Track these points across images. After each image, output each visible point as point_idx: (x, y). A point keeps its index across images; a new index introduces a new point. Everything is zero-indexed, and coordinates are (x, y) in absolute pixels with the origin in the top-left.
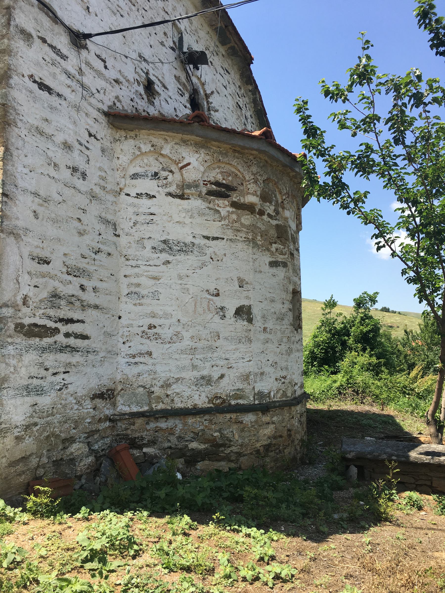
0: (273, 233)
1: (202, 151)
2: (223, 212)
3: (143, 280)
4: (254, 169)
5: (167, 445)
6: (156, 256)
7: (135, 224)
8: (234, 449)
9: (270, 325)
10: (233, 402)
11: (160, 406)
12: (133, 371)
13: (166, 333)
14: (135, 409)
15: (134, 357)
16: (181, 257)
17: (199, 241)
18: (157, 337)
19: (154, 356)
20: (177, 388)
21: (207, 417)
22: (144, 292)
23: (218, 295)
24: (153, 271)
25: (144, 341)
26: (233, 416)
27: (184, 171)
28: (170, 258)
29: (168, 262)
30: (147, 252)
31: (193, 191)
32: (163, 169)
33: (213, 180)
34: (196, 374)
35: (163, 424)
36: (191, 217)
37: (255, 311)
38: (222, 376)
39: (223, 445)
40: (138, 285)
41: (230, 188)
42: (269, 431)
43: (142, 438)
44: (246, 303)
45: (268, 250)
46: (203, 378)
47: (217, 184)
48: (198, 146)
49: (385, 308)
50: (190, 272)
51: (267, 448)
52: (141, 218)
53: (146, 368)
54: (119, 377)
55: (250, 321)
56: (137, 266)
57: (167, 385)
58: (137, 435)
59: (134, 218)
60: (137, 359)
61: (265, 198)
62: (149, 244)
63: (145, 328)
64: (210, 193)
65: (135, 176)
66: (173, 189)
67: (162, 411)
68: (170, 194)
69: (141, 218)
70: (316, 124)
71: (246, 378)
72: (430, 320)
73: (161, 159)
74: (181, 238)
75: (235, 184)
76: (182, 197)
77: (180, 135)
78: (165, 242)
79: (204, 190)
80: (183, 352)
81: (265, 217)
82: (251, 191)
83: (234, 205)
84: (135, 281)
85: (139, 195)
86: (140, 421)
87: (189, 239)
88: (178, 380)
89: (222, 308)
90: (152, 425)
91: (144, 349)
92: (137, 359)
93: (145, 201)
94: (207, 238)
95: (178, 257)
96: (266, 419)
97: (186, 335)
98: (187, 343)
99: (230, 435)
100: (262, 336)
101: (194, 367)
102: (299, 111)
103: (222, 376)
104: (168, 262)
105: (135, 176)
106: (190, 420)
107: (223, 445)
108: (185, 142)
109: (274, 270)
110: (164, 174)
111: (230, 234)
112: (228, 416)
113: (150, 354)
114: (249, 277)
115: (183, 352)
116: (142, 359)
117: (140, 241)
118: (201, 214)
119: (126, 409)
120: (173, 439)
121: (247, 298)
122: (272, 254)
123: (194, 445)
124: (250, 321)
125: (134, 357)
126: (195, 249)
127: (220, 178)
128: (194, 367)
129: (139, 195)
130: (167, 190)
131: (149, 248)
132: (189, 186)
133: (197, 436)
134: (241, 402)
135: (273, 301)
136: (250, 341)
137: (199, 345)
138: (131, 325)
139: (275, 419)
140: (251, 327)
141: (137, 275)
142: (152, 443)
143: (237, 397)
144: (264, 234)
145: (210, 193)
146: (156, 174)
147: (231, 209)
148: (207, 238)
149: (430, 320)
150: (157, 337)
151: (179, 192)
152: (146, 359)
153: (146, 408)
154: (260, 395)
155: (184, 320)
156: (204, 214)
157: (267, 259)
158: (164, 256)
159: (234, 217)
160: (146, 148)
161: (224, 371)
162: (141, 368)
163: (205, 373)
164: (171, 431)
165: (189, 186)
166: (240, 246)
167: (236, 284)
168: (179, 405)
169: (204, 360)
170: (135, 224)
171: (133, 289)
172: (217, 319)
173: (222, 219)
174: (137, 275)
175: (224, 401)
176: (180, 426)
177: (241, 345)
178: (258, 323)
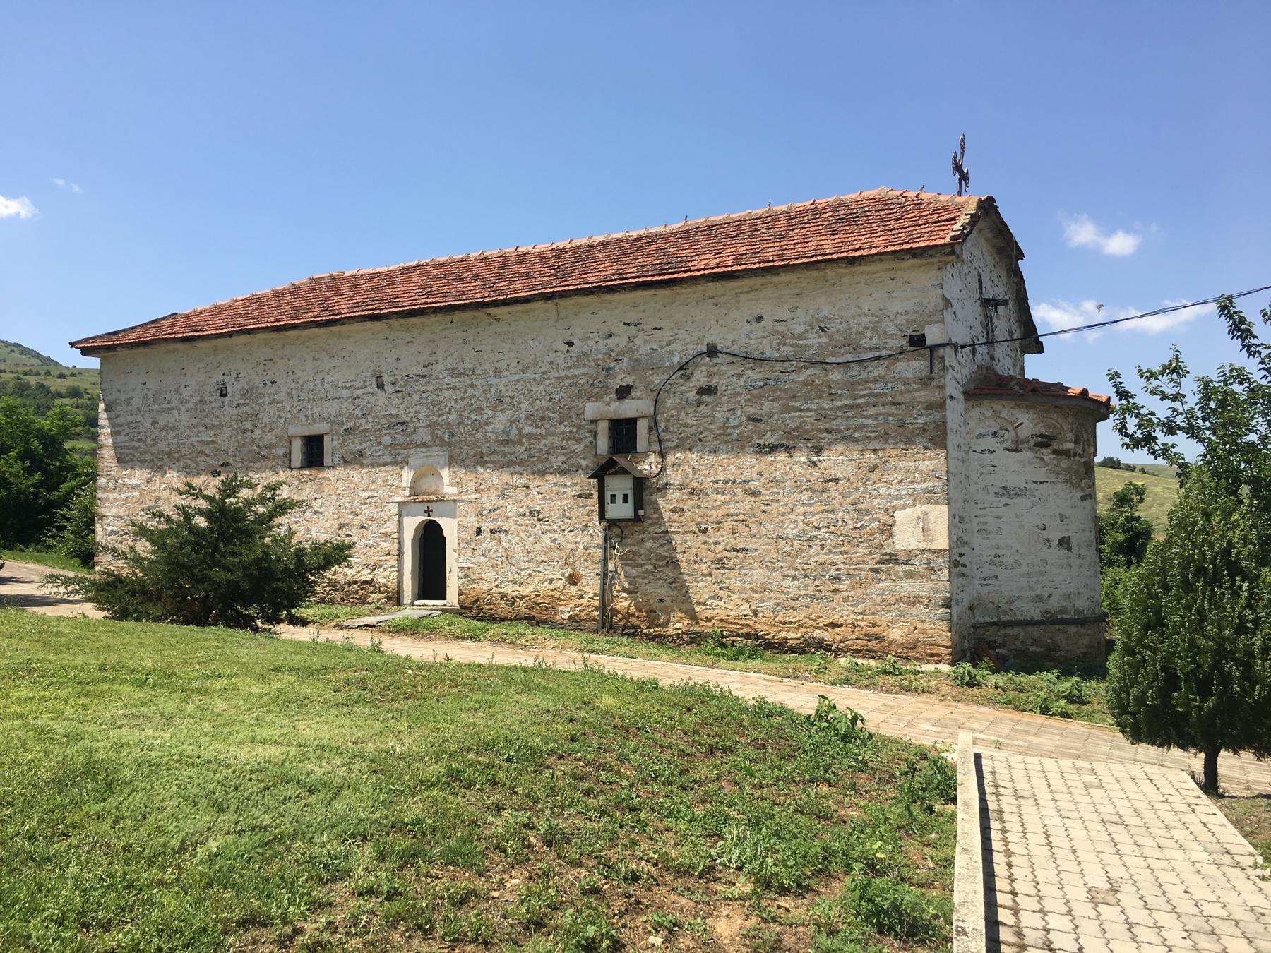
0: (1082, 470)
1: (1031, 412)
2: (1047, 460)
3: (988, 519)
4: (1070, 420)
5: (1013, 647)
6: (998, 499)
7: (981, 475)
8: (1063, 653)
9: (1082, 552)
10: (1059, 617)
11: (1006, 618)
12: (984, 590)
13: (1008, 561)
14: (988, 620)
15: (985, 579)
16: (1017, 500)
17: (1029, 486)
18: (1001, 564)
19: (1000, 578)
20: (1017, 604)
21: (1042, 627)
22: (990, 529)
23: (1045, 529)
24: (997, 512)
25: (991, 567)
26: (1061, 627)
27: (1018, 429)
28: (1009, 501)
29: (1007, 504)
30: (992, 497)
31: (1026, 445)
32: (1001, 429)
33: (1038, 433)
34: (1034, 594)
35: (1010, 632)
36: (1024, 467)
37: (1074, 542)
38: (1050, 595)
39: (1053, 650)
40: (985, 523)
41: (1052, 438)
42: (1085, 641)
43: (996, 642)
44: (1066, 534)
45: (1080, 486)
46: (1037, 596)
47: (1042, 436)
48: (1029, 408)
49: (1111, 459)
50: (1024, 512)
51: (1085, 654)
52: (985, 470)
53: (994, 588)
54: (975, 595)
55: (1070, 549)
56: (984, 508)
57: (1010, 602)
58: (991, 639)
59: (981, 470)
60: (987, 582)
61: (1076, 442)
62: (992, 491)
63: (992, 557)
64: (1036, 445)
65: (980, 436)
66: (1009, 444)
67: (1008, 621)
68: (1007, 449)
69: (985, 470)
70: (1128, 389)
71: (1068, 596)
72: (237, 707)
73: (999, 420)
74: (1017, 485)
75: (1055, 434)
76: (1016, 450)
77: (1013, 402)
78: (1004, 488)
79: (1032, 443)
80: (1021, 576)
81: (1077, 458)
82: (1069, 439)
83: (1055, 452)
84: (982, 520)
85: (983, 451)
86: (993, 629)
87: (1023, 485)
88: (1018, 597)
89: (1048, 540)
90: (1002, 632)
91: (992, 573)
92: (987, 582)
93: (987, 456)
94: (1036, 482)
95: (1014, 500)
96: (1083, 631)
97: (1024, 562)
98: (1024, 569)
99: (1059, 642)
100: (1078, 562)
101: (1031, 588)
102: (1111, 379)
103: (1050, 595)
104: (1007, 504)
105: (980, 436)
106: (1030, 629)
107: (1053, 650)
108: (1018, 406)
109: (1084, 503)
110: (1002, 432)
111: (1052, 478)
112: (1057, 627)
113: (996, 577)
114: (1067, 513)
115: (1021, 576)
116: (990, 582)
117: (985, 488)
118: (1031, 463)
119: (981, 620)
120: (1018, 643)
121: (1067, 530)
122: (1083, 489)
123: (1033, 648)
124: (1070, 549)
125: (985, 579)
126: (1028, 493)
127: (1043, 430)
128: (1031, 588)
129: (983, 451)
130: (1004, 446)
131: (992, 493)
132: (1023, 442)
133: (1035, 642)
134: (1064, 616)
135: (1083, 531)
136: (1070, 566)
137: (1033, 570)
138: (982, 555)
139: (1090, 632)
140: (1070, 554)
141: (985, 516)
142: (1003, 645)
143: (1062, 612)
144: (1076, 473)
145: (1036, 445)
146: (995, 433)
147: (1052, 456)
148: (1036, 482)
149: (237, 707)
150: (1001, 564)
151: (1014, 447)
152: (993, 581)
153: (995, 619)
154: (1078, 611)
155: (1021, 550)
156: (1032, 463)
157: (1080, 494)
158: (1004, 500)
159: (1055, 462)
160: (989, 413)
161: (1052, 591)
162: (990, 588)
163: (1038, 592)
164: (1016, 637)
165: (1023, 442)
166: (1060, 486)
167: (1059, 519)
168: (1020, 617)
169: (1037, 582)
170: (981, 475)
171: (982, 527)
172: (1045, 548)
173: (1046, 465)
174: (985, 516)
175: (1052, 615)
176: (1023, 633)
177: (1063, 570)
178: (1075, 550)
